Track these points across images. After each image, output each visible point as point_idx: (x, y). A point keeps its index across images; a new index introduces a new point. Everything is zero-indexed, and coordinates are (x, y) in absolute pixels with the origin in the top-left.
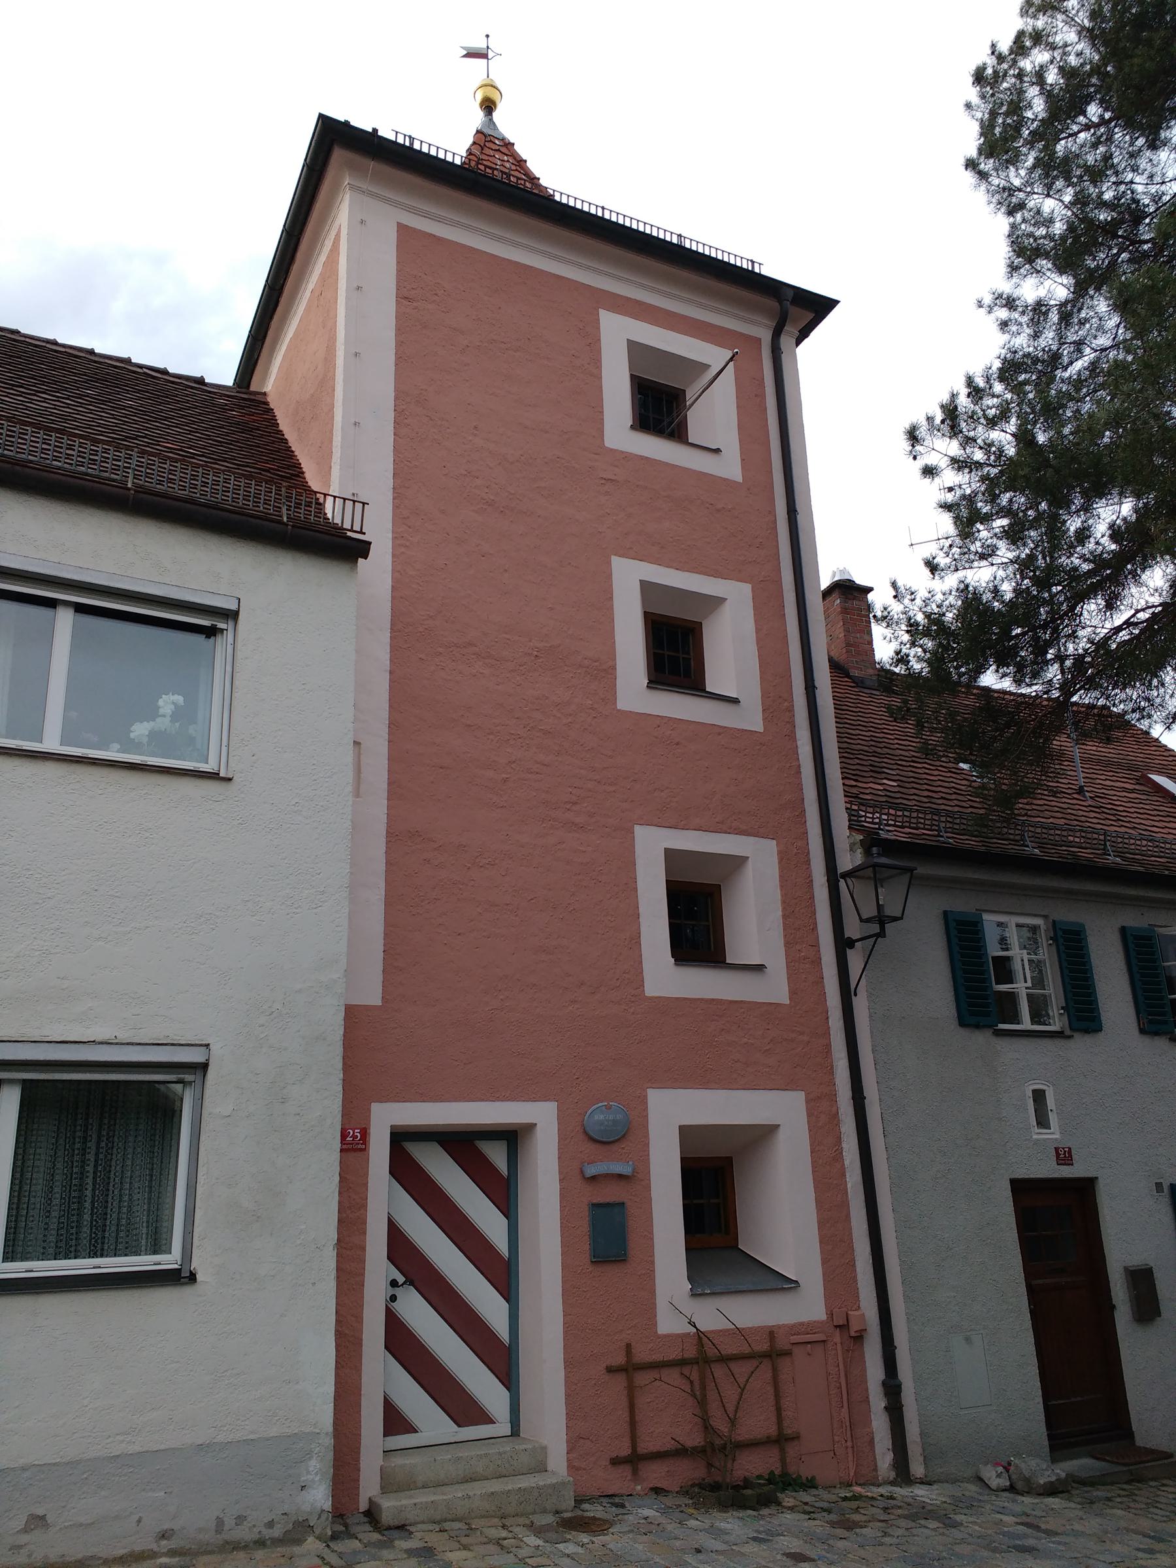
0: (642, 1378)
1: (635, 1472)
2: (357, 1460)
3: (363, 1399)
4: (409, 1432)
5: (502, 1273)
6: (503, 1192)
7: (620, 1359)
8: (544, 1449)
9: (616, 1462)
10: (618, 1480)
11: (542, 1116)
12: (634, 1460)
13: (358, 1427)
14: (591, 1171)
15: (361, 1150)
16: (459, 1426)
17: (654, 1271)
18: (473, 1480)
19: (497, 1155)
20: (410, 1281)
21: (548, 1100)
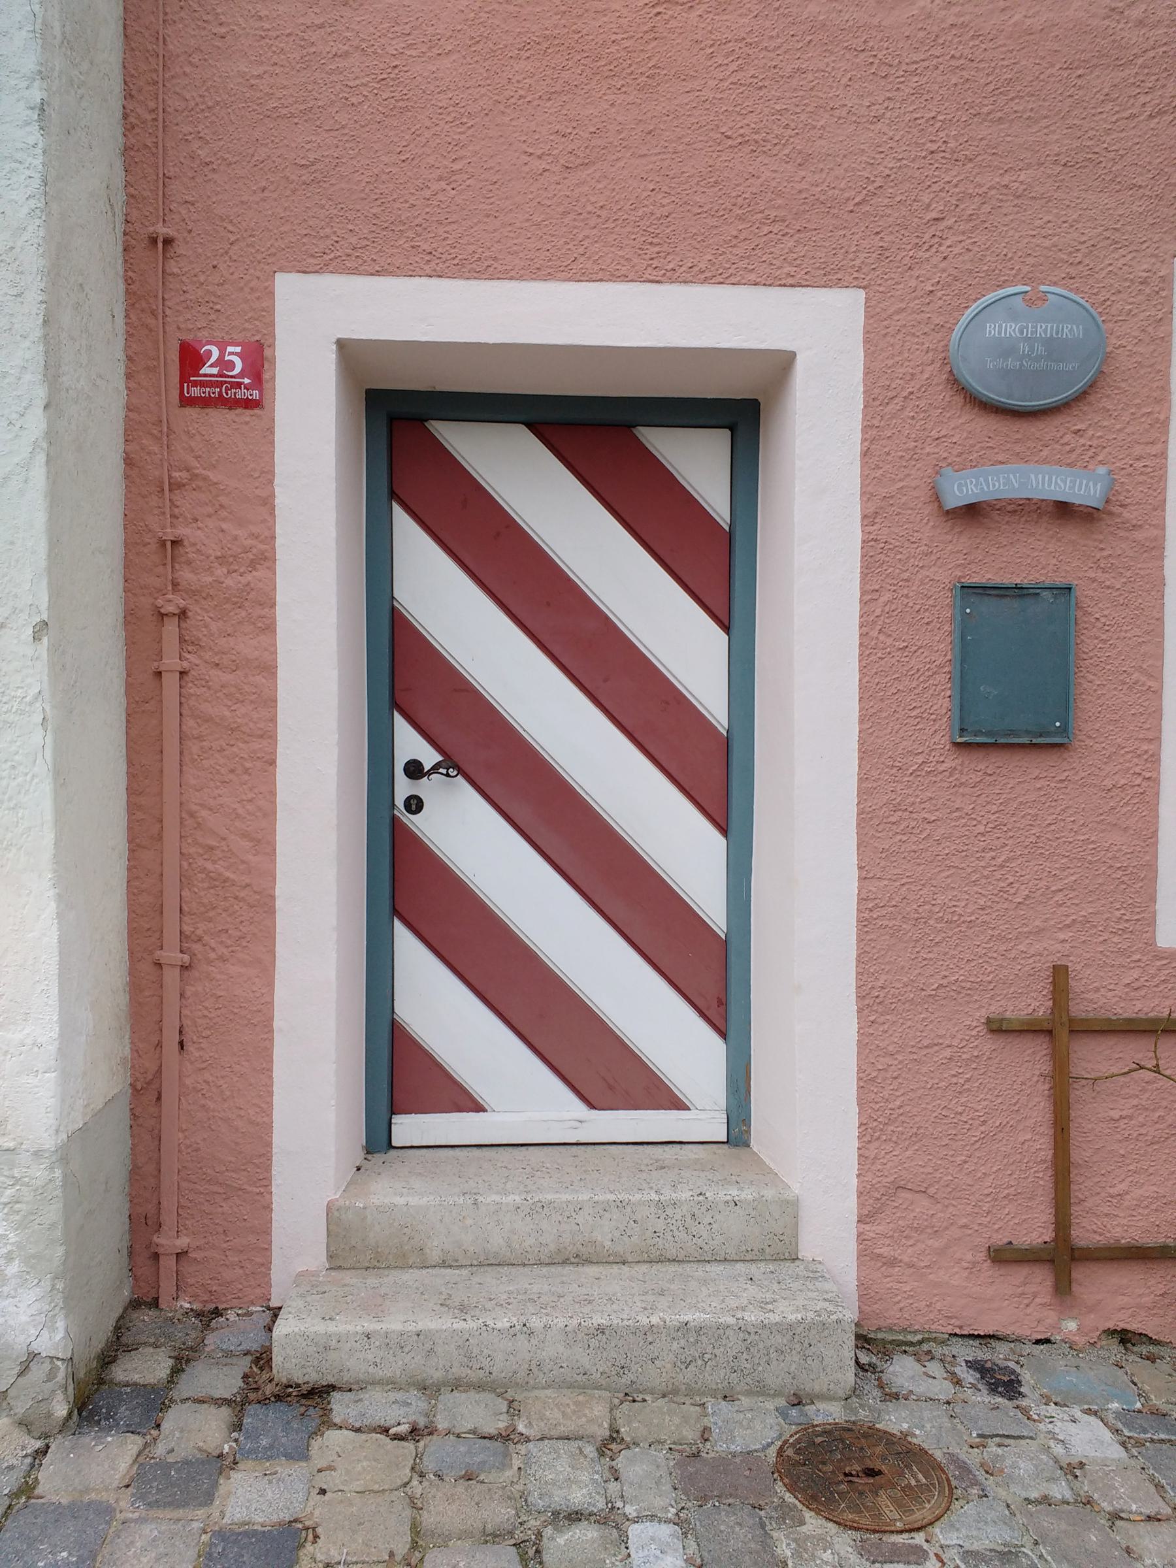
0: (1092, 1058)
1: (1063, 1288)
2: (264, 1181)
3: (278, 1038)
4: (460, 1110)
5: (711, 767)
6: (714, 563)
7: (1034, 1003)
8: (791, 1208)
9: (1004, 1256)
10: (1015, 1304)
11: (816, 339)
12: (1062, 1259)
13: (266, 1109)
14: (963, 489)
15: (249, 404)
16: (592, 1106)
17: (1155, 781)
18: (580, 1260)
19: (698, 464)
20: (451, 764)
21: (839, 284)
